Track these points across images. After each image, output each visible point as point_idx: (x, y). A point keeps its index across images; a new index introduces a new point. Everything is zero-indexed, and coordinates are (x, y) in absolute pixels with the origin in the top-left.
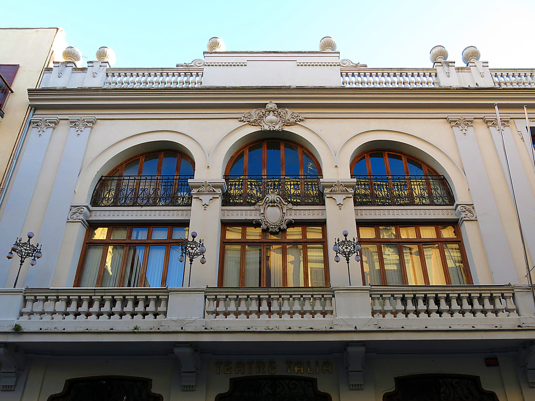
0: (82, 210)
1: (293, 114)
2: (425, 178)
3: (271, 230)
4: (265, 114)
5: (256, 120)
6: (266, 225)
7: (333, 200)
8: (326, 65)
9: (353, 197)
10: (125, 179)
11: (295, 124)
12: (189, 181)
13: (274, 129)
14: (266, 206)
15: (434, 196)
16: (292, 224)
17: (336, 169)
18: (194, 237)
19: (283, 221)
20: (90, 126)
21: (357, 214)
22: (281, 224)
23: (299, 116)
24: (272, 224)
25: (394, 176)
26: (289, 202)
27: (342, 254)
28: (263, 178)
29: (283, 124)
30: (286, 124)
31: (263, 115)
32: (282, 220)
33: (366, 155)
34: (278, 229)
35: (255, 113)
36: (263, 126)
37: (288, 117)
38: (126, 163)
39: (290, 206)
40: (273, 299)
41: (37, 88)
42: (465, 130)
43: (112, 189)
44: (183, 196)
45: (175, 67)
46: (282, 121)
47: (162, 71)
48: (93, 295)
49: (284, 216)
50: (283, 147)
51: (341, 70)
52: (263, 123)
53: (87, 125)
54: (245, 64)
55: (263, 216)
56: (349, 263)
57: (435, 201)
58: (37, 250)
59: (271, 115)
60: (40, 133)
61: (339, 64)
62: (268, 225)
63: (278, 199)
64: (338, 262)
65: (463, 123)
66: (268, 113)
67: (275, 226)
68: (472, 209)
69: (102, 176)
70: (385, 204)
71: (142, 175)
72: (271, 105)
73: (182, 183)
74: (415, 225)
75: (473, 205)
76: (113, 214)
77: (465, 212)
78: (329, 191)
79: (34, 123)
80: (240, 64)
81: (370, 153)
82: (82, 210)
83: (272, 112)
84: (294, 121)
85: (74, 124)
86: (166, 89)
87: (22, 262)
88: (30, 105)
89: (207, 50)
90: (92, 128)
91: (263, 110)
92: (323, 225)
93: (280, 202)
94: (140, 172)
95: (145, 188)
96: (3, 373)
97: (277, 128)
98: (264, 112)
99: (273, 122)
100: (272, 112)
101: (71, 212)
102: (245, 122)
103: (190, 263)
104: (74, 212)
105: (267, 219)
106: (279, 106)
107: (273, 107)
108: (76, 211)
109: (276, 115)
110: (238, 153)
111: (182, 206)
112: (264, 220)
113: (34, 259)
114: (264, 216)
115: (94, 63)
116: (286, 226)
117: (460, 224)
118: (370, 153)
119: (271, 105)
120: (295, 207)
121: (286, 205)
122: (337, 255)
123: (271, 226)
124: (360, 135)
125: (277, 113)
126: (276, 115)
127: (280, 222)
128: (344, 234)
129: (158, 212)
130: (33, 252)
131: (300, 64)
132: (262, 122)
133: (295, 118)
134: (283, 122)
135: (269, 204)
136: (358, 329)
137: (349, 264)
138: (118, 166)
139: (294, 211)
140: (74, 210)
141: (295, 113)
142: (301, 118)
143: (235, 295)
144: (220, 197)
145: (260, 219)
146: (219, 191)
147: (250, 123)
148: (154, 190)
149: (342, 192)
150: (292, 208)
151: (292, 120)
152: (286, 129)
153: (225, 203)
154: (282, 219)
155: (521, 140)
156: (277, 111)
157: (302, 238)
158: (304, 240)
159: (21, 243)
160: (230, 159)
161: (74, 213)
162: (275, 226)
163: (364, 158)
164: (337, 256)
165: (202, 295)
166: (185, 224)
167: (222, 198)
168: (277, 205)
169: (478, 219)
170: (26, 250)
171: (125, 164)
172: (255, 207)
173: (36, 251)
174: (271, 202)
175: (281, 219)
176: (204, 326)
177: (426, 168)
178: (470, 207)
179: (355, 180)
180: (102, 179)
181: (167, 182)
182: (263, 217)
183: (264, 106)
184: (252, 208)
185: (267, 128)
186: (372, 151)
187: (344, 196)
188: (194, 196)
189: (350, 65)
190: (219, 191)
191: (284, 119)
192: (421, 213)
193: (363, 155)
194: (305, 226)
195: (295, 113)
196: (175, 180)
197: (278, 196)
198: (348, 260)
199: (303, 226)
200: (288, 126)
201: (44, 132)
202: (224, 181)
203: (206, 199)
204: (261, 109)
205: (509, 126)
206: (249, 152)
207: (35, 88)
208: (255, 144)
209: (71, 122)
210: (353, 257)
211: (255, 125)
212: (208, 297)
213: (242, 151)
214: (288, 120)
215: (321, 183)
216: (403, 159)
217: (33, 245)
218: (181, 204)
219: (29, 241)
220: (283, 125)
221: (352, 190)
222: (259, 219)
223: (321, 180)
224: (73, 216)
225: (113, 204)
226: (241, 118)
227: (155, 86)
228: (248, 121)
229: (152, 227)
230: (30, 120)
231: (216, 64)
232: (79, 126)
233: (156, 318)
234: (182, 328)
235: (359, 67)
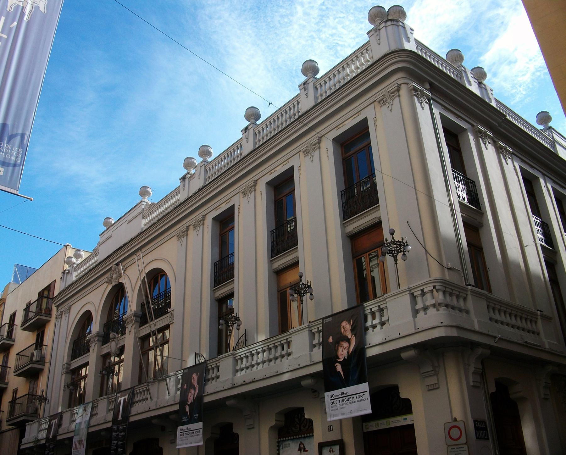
53: (393, 96)
56: (397, 263)
69: (341, 192)
86: (162, 218)
87: (396, 260)
96: (423, 373)
113: (404, 254)
143: (272, 344)
155: (327, 158)
159: (388, 243)
170: (394, 248)
173: (403, 246)
207: (30, 310)
219: (393, 238)
227: (159, 217)
233: (426, 314)
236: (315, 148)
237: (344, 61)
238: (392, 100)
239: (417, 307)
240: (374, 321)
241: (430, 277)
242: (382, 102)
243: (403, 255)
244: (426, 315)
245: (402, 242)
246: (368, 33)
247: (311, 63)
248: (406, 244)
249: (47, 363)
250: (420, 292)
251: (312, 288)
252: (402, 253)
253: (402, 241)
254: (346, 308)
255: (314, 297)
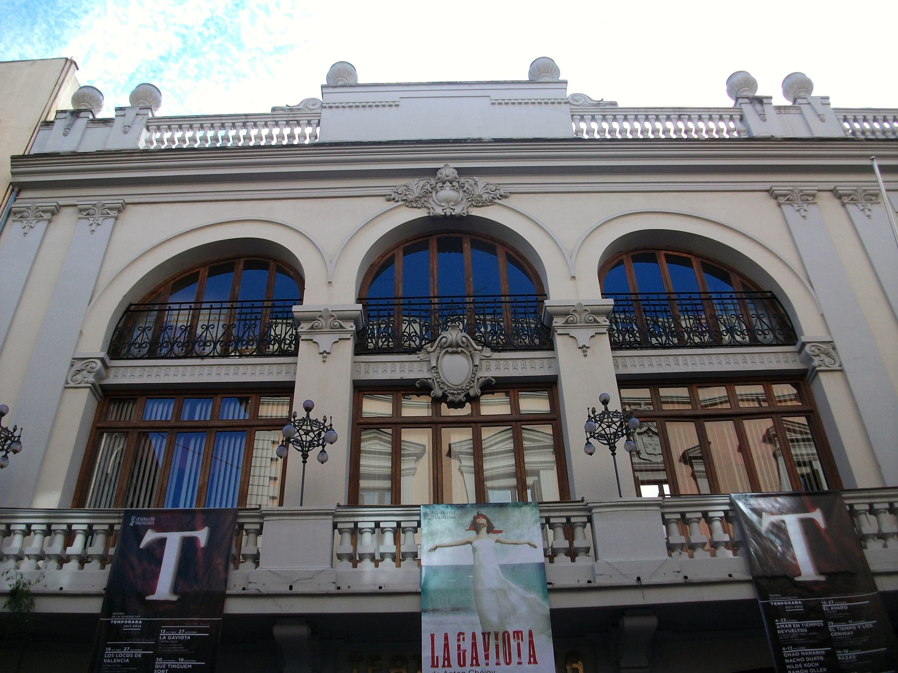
0: (94, 365)
1: (488, 186)
2: (717, 296)
3: (450, 398)
4: (436, 187)
5: (418, 197)
6: (441, 389)
7: (571, 339)
8: (523, 103)
9: (607, 333)
10: (213, 307)
11: (491, 202)
12: (295, 308)
13: (453, 214)
14: (440, 353)
15: (758, 330)
16: (490, 387)
17: (572, 282)
18: (308, 409)
19: (473, 381)
20: (115, 215)
21: (616, 366)
22: (471, 387)
23: (499, 190)
24: (453, 387)
25: (680, 295)
26: (486, 344)
27: (598, 439)
28: (433, 302)
29: (470, 203)
30: (475, 204)
31: (432, 188)
32: (473, 379)
33: (624, 257)
34: (464, 396)
35: (418, 186)
36: (433, 208)
37: (479, 190)
38: (174, 279)
39: (487, 352)
40: (404, 530)
41: (26, 154)
42: (804, 210)
43: (147, 327)
44: (216, 340)
45: (269, 111)
46: (467, 199)
47: (246, 120)
48: (116, 524)
49: (476, 371)
50: (469, 247)
51: (571, 110)
52: (433, 203)
53: (108, 214)
54: (397, 103)
55: (435, 373)
56: (615, 454)
57: (760, 338)
58: (13, 438)
59: (448, 188)
60: (26, 230)
61: (566, 101)
62: (446, 389)
63: (464, 339)
64: (591, 454)
65: (799, 198)
66: (440, 184)
67: (459, 391)
68: (832, 351)
70: (624, 346)
71: (203, 301)
72: (448, 170)
73: (255, 315)
74: (726, 382)
75: (832, 342)
76: (149, 374)
77: (818, 355)
78: (563, 323)
79: (15, 213)
80: (387, 104)
81: (632, 254)
82: (94, 365)
83: (448, 184)
84: (491, 198)
85: (85, 212)
88: (11, 183)
89: (325, 83)
90: (116, 218)
91: (432, 180)
92: (551, 387)
93: (467, 346)
94: (200, 294)
95: (209, 325)
97: (458, 211)
98: (434, 183)
99: (450, 201)
100: (448, 184)
101: (73, 369)
102: (398, 201)
103: (303, 462)
104: (78, 369)
105: (443, 378)
106: (461, 171)
107: (451, 174)
108: (83, 367)
109: (455, 189)
110: (383, 257)
111: (213, 357)
112: (438, 380)
113: (323, 451)
114: (438, 372)
115: (127, 110)
116: (480, 391)
117: (811, 379)
118: (632, 254)
119: (448, 170)
120: (496, 355)
121: (480, 351)
122: (588, 442)
123: (452, 391)
124: (610, 224)
125: (458, 185)
126: (455, 188)
127: (469, 382)
128: (602, 400)
129: (267, 367)
130: (5, 443)
131: (496, 102)
132: (431, 201)
133: (491, 194)
134: (470, 200)
135: (447, 349)
136: (644, 581)
137: (616, 456)
138: (161, 286)
139: (494, 361)
140: (79, 365)
141: (491, 184)
142: (502, 192)
144: (352, 338)
145: (430, 379)
146: (350, 326)
147: (410, 204)
148: (225, 328)
149: (586, 324)
150: (490, 356)
151: (485, 196)
152: (476, 212)
153: (360, 349)
154: (472, 377)
156: (458, 182)
157: (510, 413)
158: (515, 417)
160: (369, 269)
161: (78, 372)
162: (459, 391)
163: (621, 263)
164: (588, 443)
165: (328, 522)
166: (285, 390)
167: (355, 338)
168: (461, 350)
169: (846, 367)
171: (172, 282)
172: (419, 355)
173: (11, 440)
174: (451, 346)
175: (470, 376)
176: (334, 583)
177: (739, 279)
178: (829, 347)
179: (611, 301)
180: (130, 309)
181: (249, 313)
182: (435, 375)
183: (434, 172)
184: (413, 357)
185: (439, 211)
186: (636, 249)
187: (592, 332)
188: (303, 337)
189: (587, 102)
190: (352, 327)
191: (471, 195)
192: (704, 361)
193: (620, 258)
194: (516, 390)
195: (491, 184)
196: (264, 309)
197: (465, 334)
198: (613, 449)
199: (395, 393)
200: (479, 207)
201: (32, 228)
202: (360, 307)
203: (325, 341)
204: (427, 179)
205: (815, 203)
206: (404, 255)
208: (416, 241)
209: (81, 211)
210: (621, 443)
211: (416, 207)
212: (339, 526)
213: (233, 261)
214: (479, 197)
215: (547, 307)
216: (694, 263)
217: (317, 419)
218: (212, 354)
220: (470, 206)
221: (606, 319)
222: (427, 379)
223: (547, 303)
224: (75, 376)
225: (257, 353)
226: (391, 195)
228: (404, 200)
229: (220, 396)
230: (9, 208)
231: (343, 105)
232: (28, 219)
234: (291, 588)
235: (603, 106)
236: (109, 214)
237: (219, 118)
238: (103, 218)
239: (70, 550)
240: (68, 548)
241: (301, 505)
242: (19, 216)
243: (3, 456)
244: (399, 568)
245: (12, 434)
246: (117, 110)
247: (739, 76)
248: (16, 439)
249: (421, 313)
250: (23, 527)
251: (591, 443)
252: (320, 448)
253: (12, 431)
254: (56, 508)
255: (8, 464)
